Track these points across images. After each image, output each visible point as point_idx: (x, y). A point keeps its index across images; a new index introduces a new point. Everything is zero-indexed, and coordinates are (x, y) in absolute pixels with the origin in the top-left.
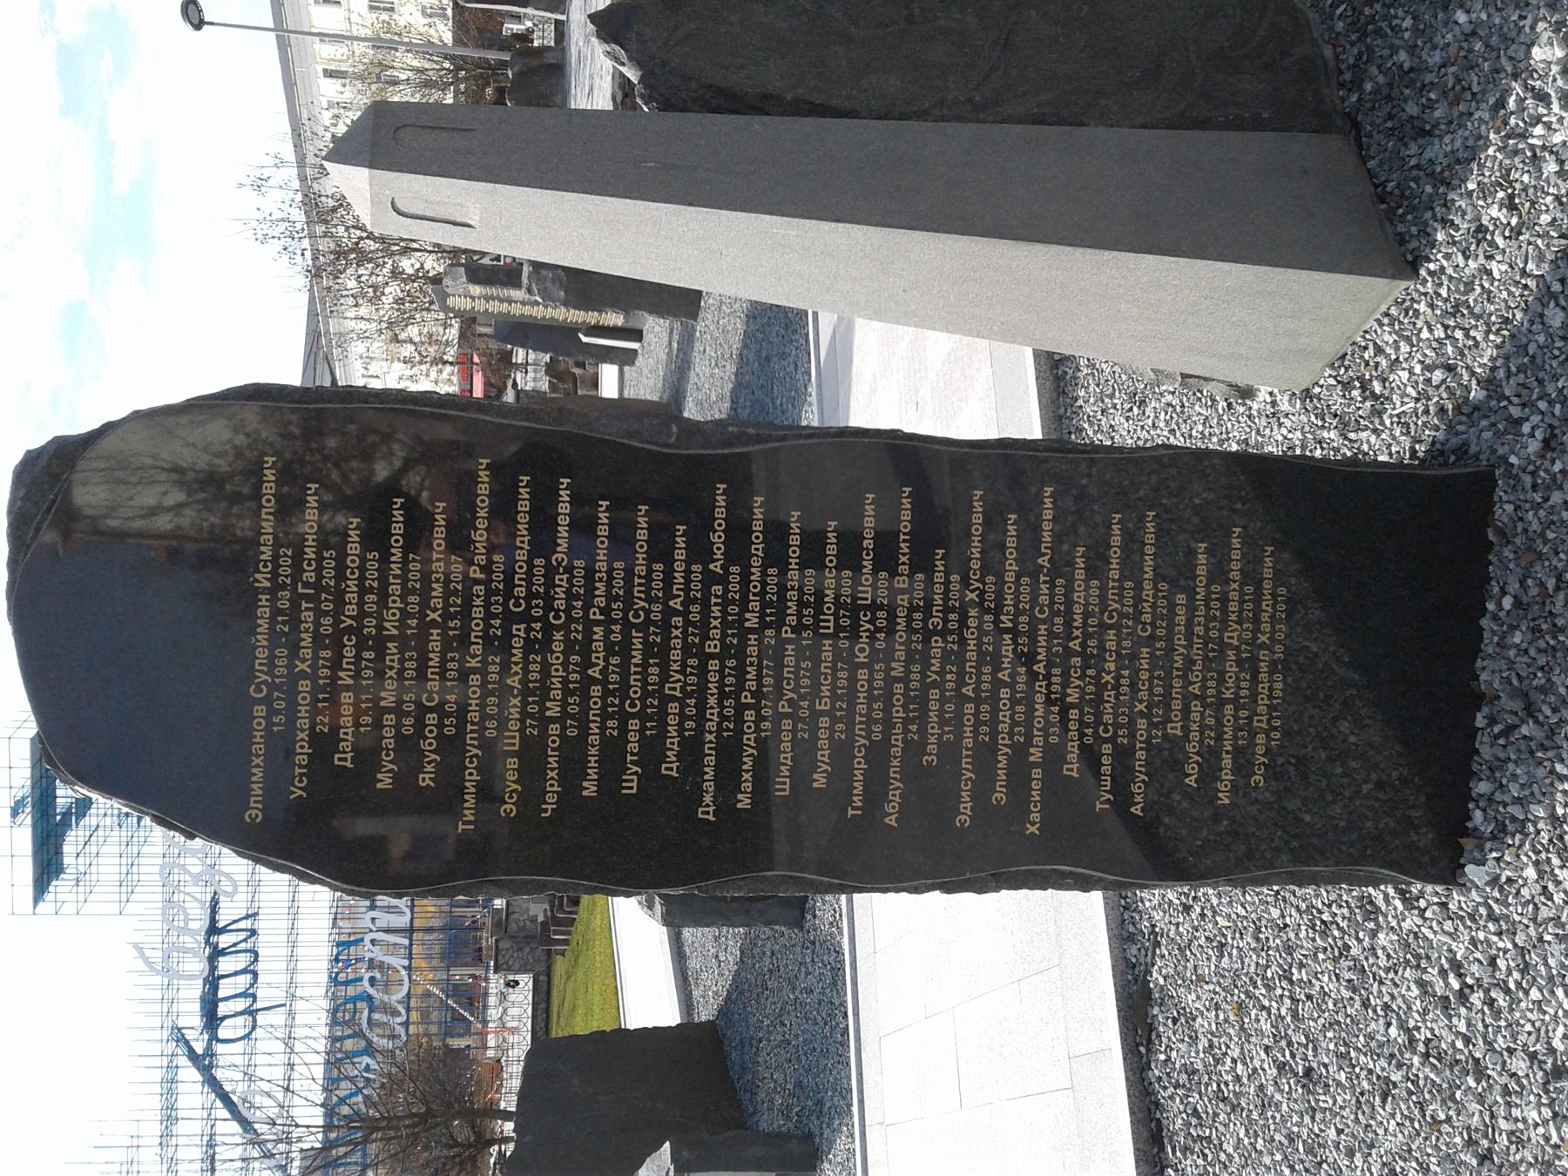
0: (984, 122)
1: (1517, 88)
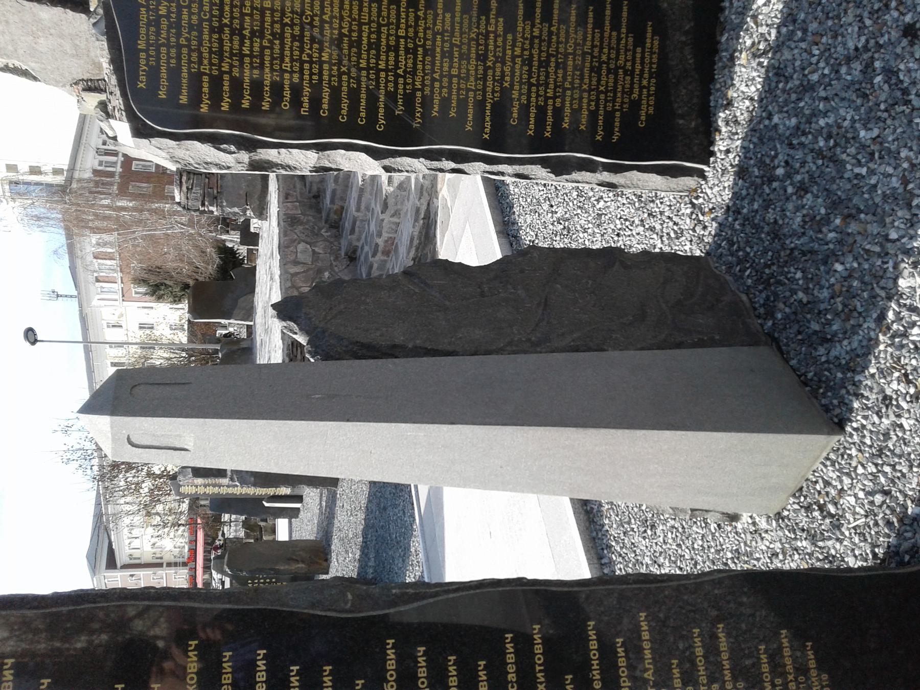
0: (541, 352)
1: (893, 305)
